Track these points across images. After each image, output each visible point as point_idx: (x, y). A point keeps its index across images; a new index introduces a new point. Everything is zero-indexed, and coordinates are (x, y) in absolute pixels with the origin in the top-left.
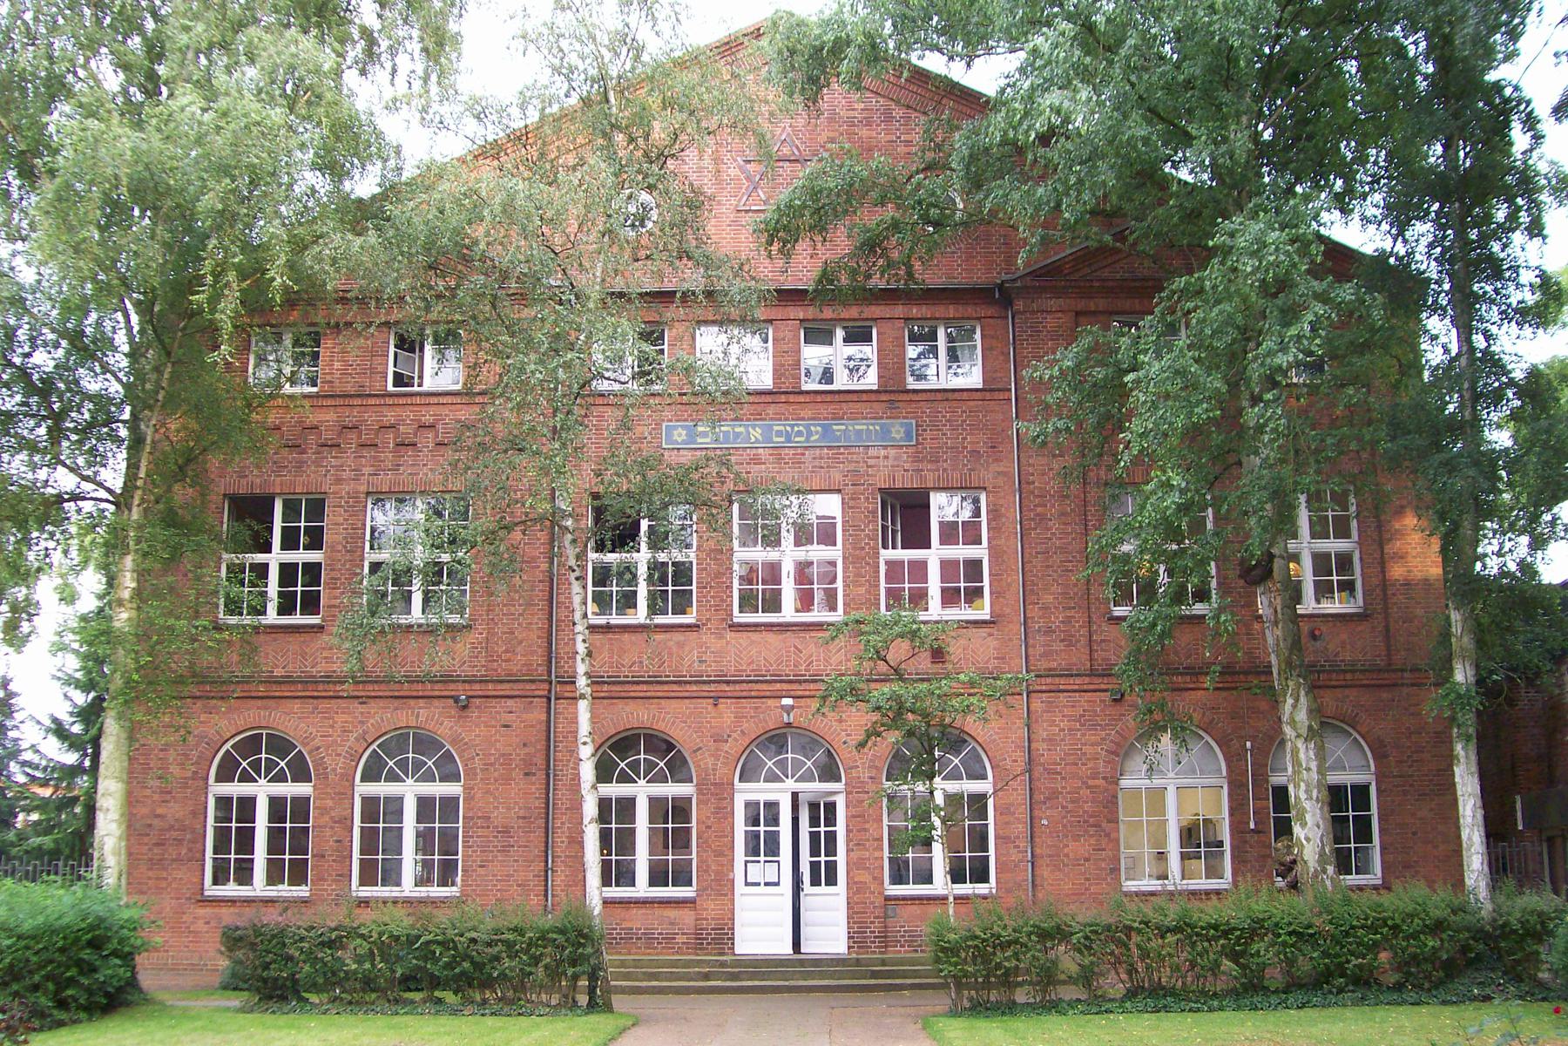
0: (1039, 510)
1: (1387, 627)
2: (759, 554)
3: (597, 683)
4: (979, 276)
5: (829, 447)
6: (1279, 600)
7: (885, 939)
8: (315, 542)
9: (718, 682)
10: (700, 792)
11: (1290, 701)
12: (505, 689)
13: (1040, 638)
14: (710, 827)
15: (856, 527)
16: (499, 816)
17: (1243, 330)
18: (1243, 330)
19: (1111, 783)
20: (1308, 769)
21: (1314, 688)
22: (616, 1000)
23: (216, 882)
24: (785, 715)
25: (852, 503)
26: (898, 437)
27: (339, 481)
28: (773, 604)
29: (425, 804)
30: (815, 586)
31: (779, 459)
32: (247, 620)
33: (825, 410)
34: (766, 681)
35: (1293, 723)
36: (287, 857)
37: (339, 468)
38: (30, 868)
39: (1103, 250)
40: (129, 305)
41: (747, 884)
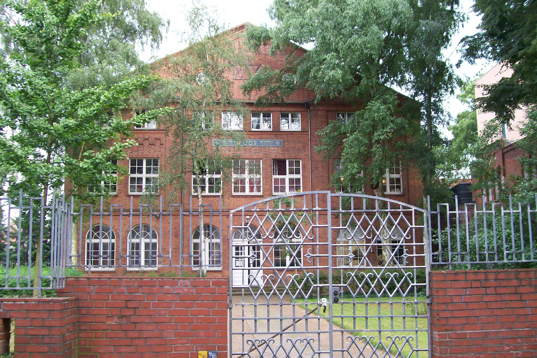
0: (316, 165)
1: (409, 198)
4: (301, 100)
5: (259, 147)
6: (380, 193)
15: (266, 169)
17: (373, 126)
18: (373, 126)
25: (265, 162)
28: (243, 190)
30: (255, 185)
31: (245, 150)
33: (257, 137)
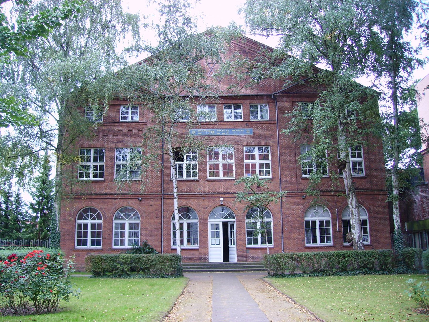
2: (213, 162)
3: (179, 194)
7: (246, 258)
8: (102, 159)
9: (204, 194)
10: (199, 221)
11: (351, 199)
12: (151, 196)
13: (284, 183)
14: (202, 230)
16: (149, 228)
19: (302, 219)
20: (355, 216)
21: (357, 195)
22: (184, 274)
23: (78, 245)
24: (221, 202)
26: (248, 133)
27: (108, 144)
28: (217, 174)
29: (93, 226)
32: (85, 179)
34: (216, 194)
35: (351, 204)
36: (82, 239)
37: (108, 141)
38: (25, 242)
39: (302, 85)
40: (56, 98)
41: (211, 245)
